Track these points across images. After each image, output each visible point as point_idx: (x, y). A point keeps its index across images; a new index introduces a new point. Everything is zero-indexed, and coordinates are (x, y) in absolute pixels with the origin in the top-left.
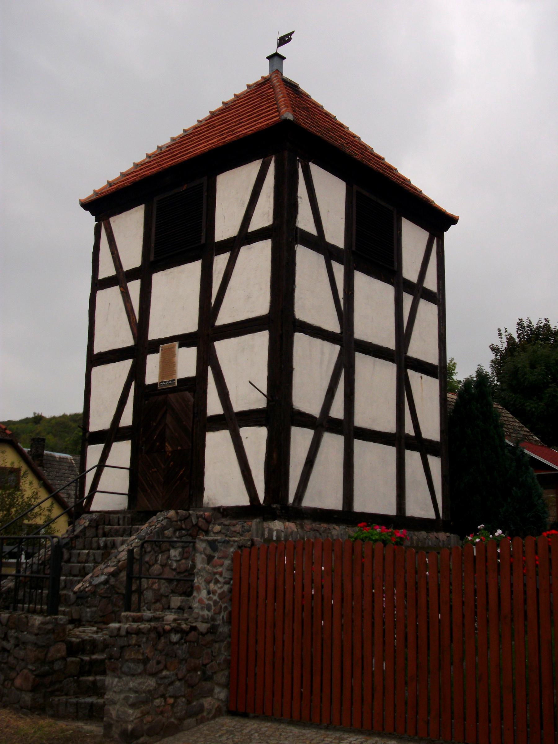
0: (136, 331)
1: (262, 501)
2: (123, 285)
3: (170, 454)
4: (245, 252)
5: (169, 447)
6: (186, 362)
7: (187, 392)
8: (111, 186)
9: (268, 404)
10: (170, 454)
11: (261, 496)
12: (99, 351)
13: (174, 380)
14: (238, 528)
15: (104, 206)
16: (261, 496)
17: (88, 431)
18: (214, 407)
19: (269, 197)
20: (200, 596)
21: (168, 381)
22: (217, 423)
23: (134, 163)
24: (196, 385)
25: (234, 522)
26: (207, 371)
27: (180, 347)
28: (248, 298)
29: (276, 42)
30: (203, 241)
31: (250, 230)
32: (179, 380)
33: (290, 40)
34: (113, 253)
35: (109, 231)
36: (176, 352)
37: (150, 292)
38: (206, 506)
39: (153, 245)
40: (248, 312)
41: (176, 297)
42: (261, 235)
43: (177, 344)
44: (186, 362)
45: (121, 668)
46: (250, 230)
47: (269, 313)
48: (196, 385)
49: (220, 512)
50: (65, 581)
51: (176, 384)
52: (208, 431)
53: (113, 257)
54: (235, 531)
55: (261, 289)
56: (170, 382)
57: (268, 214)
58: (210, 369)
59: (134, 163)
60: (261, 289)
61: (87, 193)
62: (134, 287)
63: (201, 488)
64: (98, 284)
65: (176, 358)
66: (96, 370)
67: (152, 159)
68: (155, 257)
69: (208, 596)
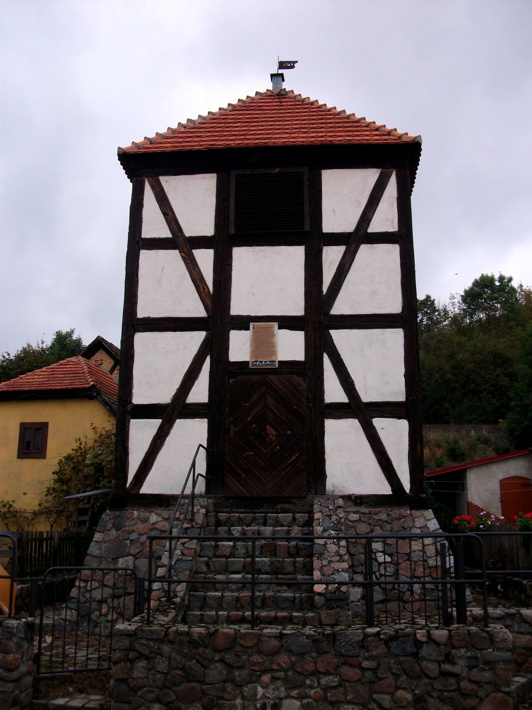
0: (209, 303)
2: (185, 250)
3: (274, 438)
4: (365, 251)
5: (272, 431)
6: (291, 346)
7: (295, 376)
8: (152, 143)
9: (406, 398)
10: (274, 438)
11: (407, 486)
12: (146, 316)
13: (275, 361)
14: (383, 516)
16: (407, 486)
17: (131, 402)
18: (334, 392)
19: (392, 206)
21: (265, 362)
22: (338, 411)
24: (307, 372)
25: (377, 510)
26: (323, 357)
27: (280, 328)
28: (374, 294)
29: (277, 65)
30: (307, 228)
31: (370, 230)
32: (280, 362)
33: (293, 67)
34: (165, 214)
35: (158, 189)
36: (276, 333)
37: (231, 265)
38: (330, 494)
39: (232, 218)
40: (374, 307)
41: (268, 278)
42: (335, 239)
43: (276, 325)
46: (370, 230)
47: (401, 313)
48: (307, 372)
49: (353, 501)
51: (277, 365)
53: (166, 219)
54: (380, 520)
55: (390, 289)
56: (268, 362)
57: (393, 220)
60: (390, 289)
61: (126, 144)
62: (205, 258)
63: (323, 476)
64: (137, 243)
65: (275, 339)
67: (187, 130)
68: (235, 231)
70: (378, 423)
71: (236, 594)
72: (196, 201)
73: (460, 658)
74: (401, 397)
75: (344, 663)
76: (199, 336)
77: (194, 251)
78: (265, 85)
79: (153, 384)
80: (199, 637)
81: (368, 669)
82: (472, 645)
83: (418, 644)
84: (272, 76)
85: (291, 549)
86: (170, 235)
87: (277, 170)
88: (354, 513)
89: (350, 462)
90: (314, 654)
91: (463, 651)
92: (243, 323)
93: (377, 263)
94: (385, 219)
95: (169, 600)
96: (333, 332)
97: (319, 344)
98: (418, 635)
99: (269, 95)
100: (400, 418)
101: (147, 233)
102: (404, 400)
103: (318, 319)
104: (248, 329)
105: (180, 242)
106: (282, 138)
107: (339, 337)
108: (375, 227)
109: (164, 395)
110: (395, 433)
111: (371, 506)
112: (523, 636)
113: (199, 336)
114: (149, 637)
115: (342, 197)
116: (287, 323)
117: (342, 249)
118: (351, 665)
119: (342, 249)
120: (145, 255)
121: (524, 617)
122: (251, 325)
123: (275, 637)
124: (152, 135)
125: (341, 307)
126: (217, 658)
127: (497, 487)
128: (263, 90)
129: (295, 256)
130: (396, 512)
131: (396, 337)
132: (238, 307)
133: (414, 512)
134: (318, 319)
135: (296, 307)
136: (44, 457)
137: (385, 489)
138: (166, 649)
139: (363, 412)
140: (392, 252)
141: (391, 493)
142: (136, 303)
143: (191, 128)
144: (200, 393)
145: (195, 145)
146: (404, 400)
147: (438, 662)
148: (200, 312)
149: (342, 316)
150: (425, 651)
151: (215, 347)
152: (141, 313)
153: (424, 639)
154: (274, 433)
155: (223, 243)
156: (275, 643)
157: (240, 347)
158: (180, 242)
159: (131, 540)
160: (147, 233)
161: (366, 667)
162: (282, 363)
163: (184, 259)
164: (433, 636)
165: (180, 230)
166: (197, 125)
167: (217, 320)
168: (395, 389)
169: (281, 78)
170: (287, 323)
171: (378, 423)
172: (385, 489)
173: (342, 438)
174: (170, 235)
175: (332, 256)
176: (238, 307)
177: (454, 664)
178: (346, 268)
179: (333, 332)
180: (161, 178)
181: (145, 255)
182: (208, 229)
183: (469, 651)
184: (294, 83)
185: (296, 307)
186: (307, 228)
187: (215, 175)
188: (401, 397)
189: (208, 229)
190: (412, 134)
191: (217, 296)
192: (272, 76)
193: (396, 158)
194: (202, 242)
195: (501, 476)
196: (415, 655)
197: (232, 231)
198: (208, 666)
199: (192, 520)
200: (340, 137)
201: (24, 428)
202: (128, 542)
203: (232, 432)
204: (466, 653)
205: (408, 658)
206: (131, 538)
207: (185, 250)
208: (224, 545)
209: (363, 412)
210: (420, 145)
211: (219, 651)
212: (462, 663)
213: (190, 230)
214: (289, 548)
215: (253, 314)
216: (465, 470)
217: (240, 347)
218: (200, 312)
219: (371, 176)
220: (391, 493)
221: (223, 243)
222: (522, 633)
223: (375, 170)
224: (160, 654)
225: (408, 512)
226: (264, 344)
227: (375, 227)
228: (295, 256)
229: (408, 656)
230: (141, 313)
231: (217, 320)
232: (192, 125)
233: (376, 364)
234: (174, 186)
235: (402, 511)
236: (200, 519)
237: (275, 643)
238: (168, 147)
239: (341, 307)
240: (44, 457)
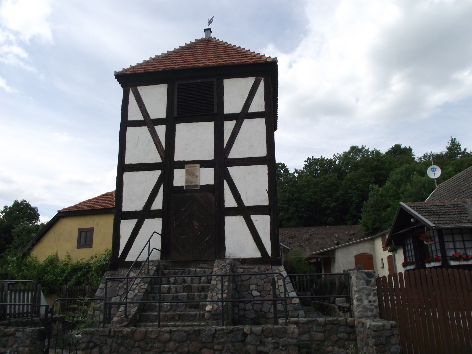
0: (163, 154)
1: (270, 255)
2: (151, 126)
4: (247, 123)
6: (207, 177)
8: (134, 69)
11: (269, 252)
14: (256, 270)
15: (131, 80)
16: (269, 252)
18: (230, 201)
20: (363, 304)
22: (232, 212)
23: (276, 58)
24: (216, 190)
30: (215, 112)
31: (249, 111)
32: (201, 186)
34: (140, 107)
41: (195, 140)
42: (231, 117)
43: (198, 165)
44: (207, 177)
45: (389, 350)
46: (249, 111)
48: (216, 190)
50: (156, 306)
52: (226, 216)
58: (225, 181)
59: (276, 58)
61: (119, 69)
62: (161, 130)
64: (126, 124)
66: (126, 175)
69: (370, 304)
70: (254, 218)
71: (165, 313)
72: (156, 99)
73: (268, 343)
74: (266, 203)
75: (204, 347)
76: (158, 173)
77: (155, 127)
78: (202, 35)
79: (133, 201)
80: (127, 334)
81: (217, 350)
82: (276, 336)
83: (245, 335)
84: (205, 30)
85: (200, 288)
86: (143, 119)
87: (199, 81)
88: (241, 268)
89: (239, 240)
90: (188, 342)
91: (270, 339)
92: (181, 165)
93: (254, 129)
94: (258, 104)
95: (126, 316)
96: (229, 168)
97: (222, 175)
98: (245, 330)
99: (202, 41)
100: (265, 214)
101: (131, 118)
102: (268, 204)
103: (221, 161)
104: (183, 168)
105: (148, 122)
106: (204, 63)
107: (233, 171)
108: (253, 109)
109: (138, 206)
110: (263, 223)
111: (250, 264)
112: (319, 334)
113: (158, 173)
114: (101, 334)
115: (235, 93)
116: (204, 164)
117: (234, 122)
118: (208, 348)
119: (234, 122)
120: (130, 130)
121: (319, 322)
122: (185, 166)
123: (167, 332)
124: (134, 64)
125: (234, 154)
126: (136, 345)
127: (353, 260)
128: (199, 38)
129: (210, 126)
130: (263, 268)
131: (263, 169)
132: (179, 156)
133: (273, 267)
134: (221, 161)
135: (209, 155)
136: (92, 247)
137: (258, 255)
138: (110, 341)
139: (245, 211)
140: (261, 123)
141: (261, 257)
142: (125, 156)
143: (156, 60)
144: (158, 204)
145: (157, 68)
146: (268, 204)
147: (256, 345)
148: (158, 159)
149: (234, 159)
150: (248, 339)
151: (166, 179)
152: (127, 162)
153: (248, 332)
154: (197, 225)
155: (170, 122)
156: (167, 336)
157: (179, 178)
158: (148, 122)
159: (120, 287)
160: (131, 118)
161: (216, 349)
162: (202, 186)
163: (150, 131)
164: (254, 331)
165: (148, 115)
166: (160, 58)
167: (168, 164)
168: (262, 199)
169: (209, 31)
170: (204, 164)
171: (254, 218)
172: (258, 255)
173: (234, 227)
174: (143, 119)
175: (229, 126)
176: (179, 156)
177: (266, 346)
178: (237, 132)
179: (229, 168)
180: (139, 88)
181: (130, 130)
182: (162, 114)
183: (274, 339)
184: (219, 34)
185: (209, 155)
186: (215, 112)
187: (166, 85)
188: (266, 203)
189: (162, 114)
190: (272, 57)
191: (168, 150)
192: (205, 30)
193: (265, 72)
194: (159, 122)
195: (355, 253)
196: (243, 341)
197: (175, 115)
198: (131, 350)
199: (148, 273)
200: (234, 61)
201: (81, 231)
202: (118, 288)
203: (174, 225)
204: (272, 340)
205: (240, 343)
206: (119, 286)
207: (151, 126)
208: (164, 287)
209: (245, 211)
210: (277, 62)
211: (137, 341)
212: (270, 346)
213: (153, 115)
214: (198, 287)
215: (186, 159)
216: (333, 251)
217: (179, 178)
218: (158, 159)
219: (250, 81)
220: (261, 257)
221: (170, 122)
222: (318, 332)
223: (253, 78)
224: (106, 344)
225: (270, 267)
226: (190, 176)
227: (253, 109)
228: (210, 126)
229: (239, 342)
230: (127, 162)
231: (168, 164)
232: (158, 58)
233: (252, 185)
234: (144, 91)
235: (267, 266)
236: (152, 272)
237: (167, 336)
238: (142, 70)
239: (234, 154)
240: (92, 247)
